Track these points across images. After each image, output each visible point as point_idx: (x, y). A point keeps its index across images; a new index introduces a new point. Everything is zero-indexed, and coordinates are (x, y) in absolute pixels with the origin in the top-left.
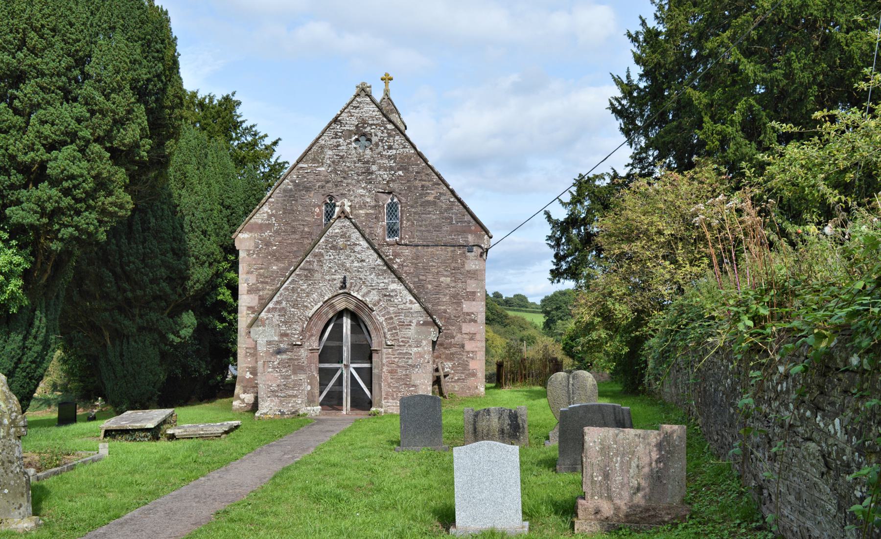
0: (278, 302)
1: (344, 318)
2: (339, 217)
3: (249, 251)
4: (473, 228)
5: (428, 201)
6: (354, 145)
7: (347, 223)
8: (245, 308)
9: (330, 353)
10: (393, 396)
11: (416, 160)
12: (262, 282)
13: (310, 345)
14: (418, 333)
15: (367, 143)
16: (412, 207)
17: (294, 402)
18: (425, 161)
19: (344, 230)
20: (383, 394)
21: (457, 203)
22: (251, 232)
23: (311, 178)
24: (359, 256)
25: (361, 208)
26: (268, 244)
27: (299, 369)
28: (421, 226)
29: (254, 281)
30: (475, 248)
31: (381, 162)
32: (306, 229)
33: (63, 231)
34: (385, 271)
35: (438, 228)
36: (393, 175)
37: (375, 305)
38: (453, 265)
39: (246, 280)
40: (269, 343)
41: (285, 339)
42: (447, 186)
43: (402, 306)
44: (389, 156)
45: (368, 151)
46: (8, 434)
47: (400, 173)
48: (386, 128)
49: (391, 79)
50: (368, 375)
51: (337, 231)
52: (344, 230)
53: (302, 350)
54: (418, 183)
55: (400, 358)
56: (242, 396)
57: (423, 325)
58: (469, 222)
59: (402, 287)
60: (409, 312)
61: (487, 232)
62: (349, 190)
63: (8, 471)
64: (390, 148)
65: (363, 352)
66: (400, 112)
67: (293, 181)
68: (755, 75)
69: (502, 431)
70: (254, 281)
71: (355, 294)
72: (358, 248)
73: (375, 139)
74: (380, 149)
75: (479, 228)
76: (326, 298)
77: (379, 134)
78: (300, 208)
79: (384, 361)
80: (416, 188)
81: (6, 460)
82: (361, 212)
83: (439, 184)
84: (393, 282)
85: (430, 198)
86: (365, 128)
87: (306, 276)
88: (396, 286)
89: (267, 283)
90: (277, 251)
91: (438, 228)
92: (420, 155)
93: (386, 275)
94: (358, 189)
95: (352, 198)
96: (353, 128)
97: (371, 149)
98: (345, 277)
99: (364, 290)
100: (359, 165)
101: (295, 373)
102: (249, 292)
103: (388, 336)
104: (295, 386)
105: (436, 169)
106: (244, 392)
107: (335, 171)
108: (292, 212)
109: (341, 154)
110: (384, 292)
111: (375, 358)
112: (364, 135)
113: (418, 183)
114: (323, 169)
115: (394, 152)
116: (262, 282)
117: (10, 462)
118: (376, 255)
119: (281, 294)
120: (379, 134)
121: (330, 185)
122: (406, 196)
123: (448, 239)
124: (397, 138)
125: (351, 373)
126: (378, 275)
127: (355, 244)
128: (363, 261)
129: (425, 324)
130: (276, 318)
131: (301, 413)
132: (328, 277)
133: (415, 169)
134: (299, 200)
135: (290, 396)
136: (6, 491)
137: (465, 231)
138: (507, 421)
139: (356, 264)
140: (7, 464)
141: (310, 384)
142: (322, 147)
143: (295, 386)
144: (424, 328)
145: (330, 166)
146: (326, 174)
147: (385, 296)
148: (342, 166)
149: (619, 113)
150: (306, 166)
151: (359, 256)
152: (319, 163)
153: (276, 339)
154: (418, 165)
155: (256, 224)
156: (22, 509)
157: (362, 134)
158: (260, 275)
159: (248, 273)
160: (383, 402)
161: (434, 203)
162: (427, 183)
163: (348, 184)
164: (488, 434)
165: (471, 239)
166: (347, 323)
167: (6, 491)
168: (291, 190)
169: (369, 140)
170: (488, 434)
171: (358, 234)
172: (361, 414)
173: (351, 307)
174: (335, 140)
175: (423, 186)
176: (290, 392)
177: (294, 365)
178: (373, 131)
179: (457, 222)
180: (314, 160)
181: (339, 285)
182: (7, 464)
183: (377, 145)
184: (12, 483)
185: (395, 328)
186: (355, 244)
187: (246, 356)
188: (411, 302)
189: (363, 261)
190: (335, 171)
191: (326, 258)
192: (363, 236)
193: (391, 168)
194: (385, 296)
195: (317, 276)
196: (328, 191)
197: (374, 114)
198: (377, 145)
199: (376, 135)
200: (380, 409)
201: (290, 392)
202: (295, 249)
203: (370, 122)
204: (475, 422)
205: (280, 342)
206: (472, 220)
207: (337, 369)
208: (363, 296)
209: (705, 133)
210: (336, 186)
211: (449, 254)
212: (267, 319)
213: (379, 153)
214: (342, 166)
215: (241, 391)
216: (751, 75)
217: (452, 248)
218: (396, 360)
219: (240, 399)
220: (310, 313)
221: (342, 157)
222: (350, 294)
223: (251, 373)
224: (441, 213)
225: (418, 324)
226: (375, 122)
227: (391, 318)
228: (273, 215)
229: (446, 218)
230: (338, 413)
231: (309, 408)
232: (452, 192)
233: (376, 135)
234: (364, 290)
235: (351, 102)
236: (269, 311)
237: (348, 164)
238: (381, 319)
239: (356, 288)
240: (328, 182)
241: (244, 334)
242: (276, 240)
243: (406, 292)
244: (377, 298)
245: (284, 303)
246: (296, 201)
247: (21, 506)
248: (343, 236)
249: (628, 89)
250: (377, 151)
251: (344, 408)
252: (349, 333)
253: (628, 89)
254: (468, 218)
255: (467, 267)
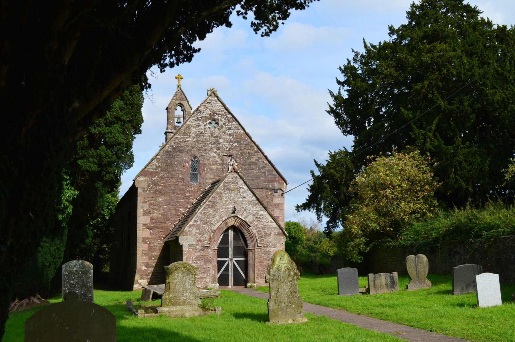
0: (195, 221)
1: (230, 231)
2: (232, 171)
3: (144, 188)
4: (277, 179)
5: (252, 162)
6: (208, 126)
7: (236, 175)
8: (141, 225)
9: (222, 252)
10: (261, 276)
11: (245, 137)
12: (152, 209)
13: (214, 247)
14: (275, 239)
15: (216, 126)
16: (243, 165)
17: (205, 281)
18: (250, 138)
19: (234, 179)
20: (256, 275)
21: (268, 164)
22: (145, 176)
23: (183, 144)
24: (242, 194)
25: (213, 164)
26: (156, 184)
27: (208, 261)
28: (248, 177)
29: (147, 208)
30: (279, 191)
31: (225, 137)
32: (180, 176)
33: (108, 176)
34: (257, 204)
35: (258, 178)
36: (232, 145)
37: (251, 223)
38: (266, 200)
39: (142, 207)
40: (190, 246)
41: (200, 243)
42: (263, 154)
43: (266, 224)
44: (230, 134)
45: (217, 130)
46: (293, 279)
47: (236, 144)
48: (227, 117)
49: (182, 78)
50: (245, 266)
51: (230, 179)
52: (234, 179)
53: (210, 250)
54: (246, 151)
55: (265, 254)
56: (140, 281)
57: (277, 235)
58: (275, 175)
59: (266, 213)
60: (270, 228)
61: (285, 182)
62: (206, 153)
63: (294, 297)
64: (230, 129)
65: (243, 251)
66: (189, 99)
67: (172, 146)
68: (445, 107)
69: (387, 285)
70: (147, 208)
71: (240, 217)
72: (242, 190)
73: (221, 123)
74: (224, 129)
75: (281, 179)
76: (224, 219)
77: (223, 120)
78: (176, 163)
79: (256, 256)
80: (245, 154)
81: (292, 291)
82: (213, 167)
83: (258, 152)
84: (261, 210)
85: (253, 160)
86: (215, 116)
87: (212, 206)
88: (263, 212)
89: (155, 209)
90: (162, 189)
91: (258, 178)
92: (247, 134)
93: (257, 206)
94: (211, 152)
95: (208, 158)
96: (208, 116)
97: (219, 129)
98: (234, 207)
99: (245, 214)
100: (212, 138)
101: (205, 264)
102: (145, 214)
103: (258, 241)
104: (205, 271)
105: (257, 143)
106: (141, 279)
107: (197, 141)
108: (171, 165)
109: (201, 131)
110: (256, 216)
111: (250, 254)
112: (214, 120)
113: (246, 151)
114: (190, 139)
115: (232, 131)
116: (152, 209)
117: (295, 292)
118: (252, 194)
119: (197, 216)
120: (223, 120)
121: (195, 149)
122: (240, 158)
123: (264, 185)
124: (234, 123)
125: (234, 264)
126: (253, 206)
127: (241, 188)
128: (244, 197)
129: (279, 234)
130: (194, 231)
131: (209, 287)
132: (225, 207)
133: (245, 142)
134: (176, 158)
135: (203, 278)
136: (293, 306)
137: (272, 181)
138: (389, 280)
139: (241, 199)
140: (293, 293)
141: (214, 270)
142: (189, 126)
143: (205, 271)
144: (278, 237)
145: (194, 138)
146: (192, 142)
147: (257, 218)
148: (202, 138)
149: (332, 111)
150: (179, 137)
151: (242, 194)
152: (187, 135)
153: (194, 243)
154: (246, 140)
155: (148, 171)
156: (301, 314)
157: (213, 119)
158: (151, 204)
159: (143, 202)
160: (256, 280)
161: (255, 163)
162: (251, 151)
163: (205, 150)
164: (381, 286)
165: (276, 185)
166: (231, 233)
167: (293, 306)
168: (170, 151)
169: (218, 124)
170: (381, 286)
171: (242, 182)
172: (241, 288)
173: (237, 224)
174: (197, 122)
175: (249, 153)
176: (202, 275)
177: (205, 259)
178: (219, 118)
179: (269, 175)
180: (184, 134)
181: (231, 211)
182: (293, 293)
183: (222, 127)
184: (296, 302)
185: (262, 237)
186: (241, 188)
187: (142, 256)
188: (271, 222)
189: (244, 197)
190: (197, 141)
191: (224, 195)
192: (245, 183)
193: (231, 141)
194: (257, 218)
195: (219, 206)
196: (194, 153)
197: (220, 108)
198: (222, 127)
199: (221, 121)
200: (253, 284)
201: (202, 275)
202: (173, 188)
203: (218, 113)
204: (374, 280)
205: (197, 245)
206: (277, 174)
207: (225, 261)
208: (245, 218)
209: (414, 134)
210: (199, 150)
211: (264, 194)
212: (189, 231)
213: (223, 132)
214: (202, 138)
215: (139, 278)
216: (443, 106)
217: (266, 190)
218: (263, 255)
219: (138, 283)
220: (215, 228)
221: (201, 133)
222: (237, 217)
223: (145, 266)
224: (259, 169)
225: (275, 234)
226: (221, 113)
227: (260, 231)
228: (159, 166)
229: (262, 173)
230: (226, 287)
231: (213, 285)
232: (266, 157)
233: (221, 121)
234: (245, 214)
235: (206, 100)
236: (190, 226)
237: (205, 137)
238: (255, 231)
239: (241, 213)
240: (193, 148)
241: (141, 241)
242: (161, 182)
243: (268, 216)
244: (252, 219)
245: (199, 222)
246: (174, 158)
247: (301, 312)
248: (233, 182)
249: (337, 98)
250: (223, 130)
251: (230, 284)
252: (232, 239)
253: (337, 98)
254: (274, 173)
255: (274, 202)
